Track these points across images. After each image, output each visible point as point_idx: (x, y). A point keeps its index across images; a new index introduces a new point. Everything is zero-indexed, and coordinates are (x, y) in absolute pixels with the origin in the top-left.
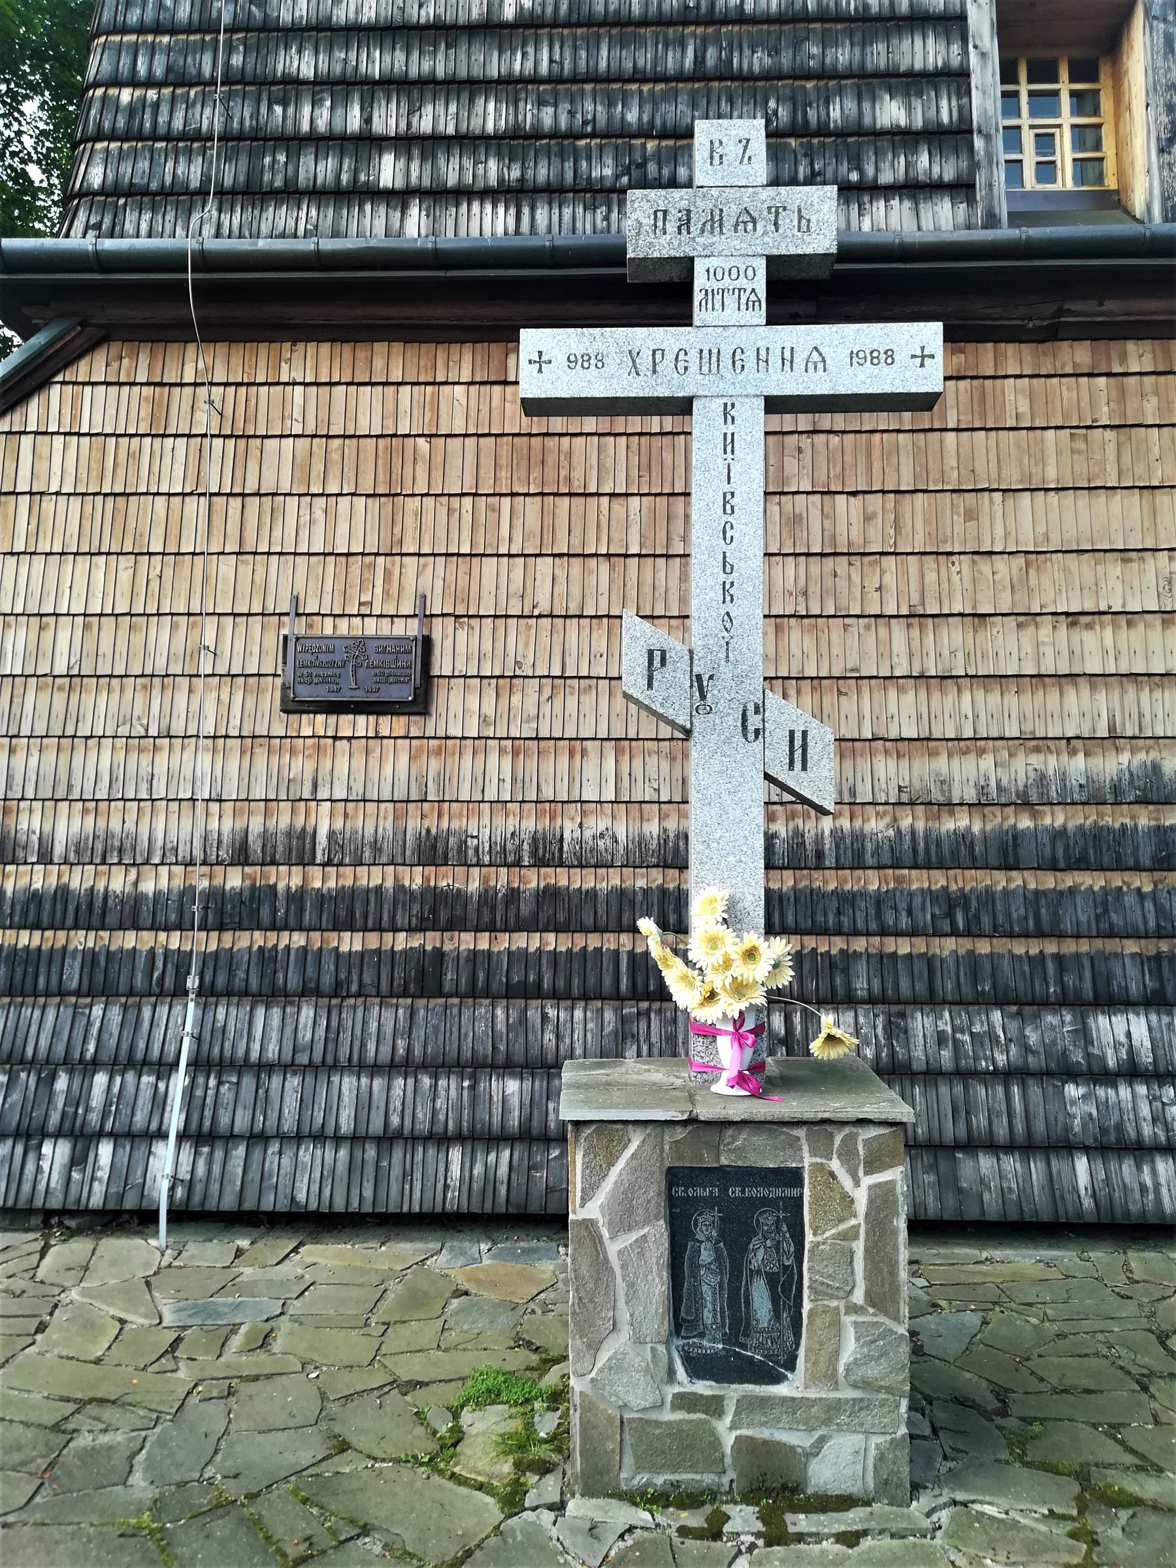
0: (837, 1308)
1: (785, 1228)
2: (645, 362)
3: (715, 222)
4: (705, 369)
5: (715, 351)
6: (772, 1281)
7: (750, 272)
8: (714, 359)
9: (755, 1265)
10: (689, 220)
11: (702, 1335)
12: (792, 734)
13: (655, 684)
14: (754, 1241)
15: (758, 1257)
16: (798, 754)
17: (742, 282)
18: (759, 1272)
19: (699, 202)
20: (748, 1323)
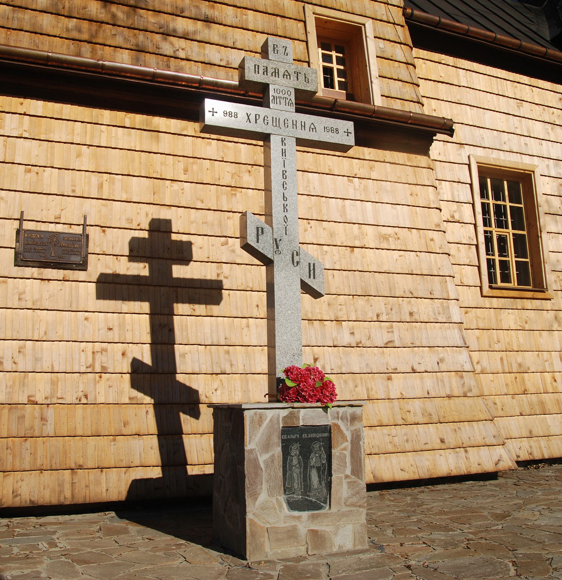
0: (342, 477)
1: (323, 449)
2: (252, 118)
3: (276, 73)
4: (274, 124)
5: (278, 118)
6: (318, 469)
7: (289, 92)
8: (277, 121)
9: (312, 464)
10: (267, 70)
11: (293, 493)
12: (309, 264)
13: (260, 241)
14: (312, 455)
15: (314, 460)
16: (312, 272)
17: (286, 96)
18: (314, 467)
19: (270, 65)
20: (310, 487)
